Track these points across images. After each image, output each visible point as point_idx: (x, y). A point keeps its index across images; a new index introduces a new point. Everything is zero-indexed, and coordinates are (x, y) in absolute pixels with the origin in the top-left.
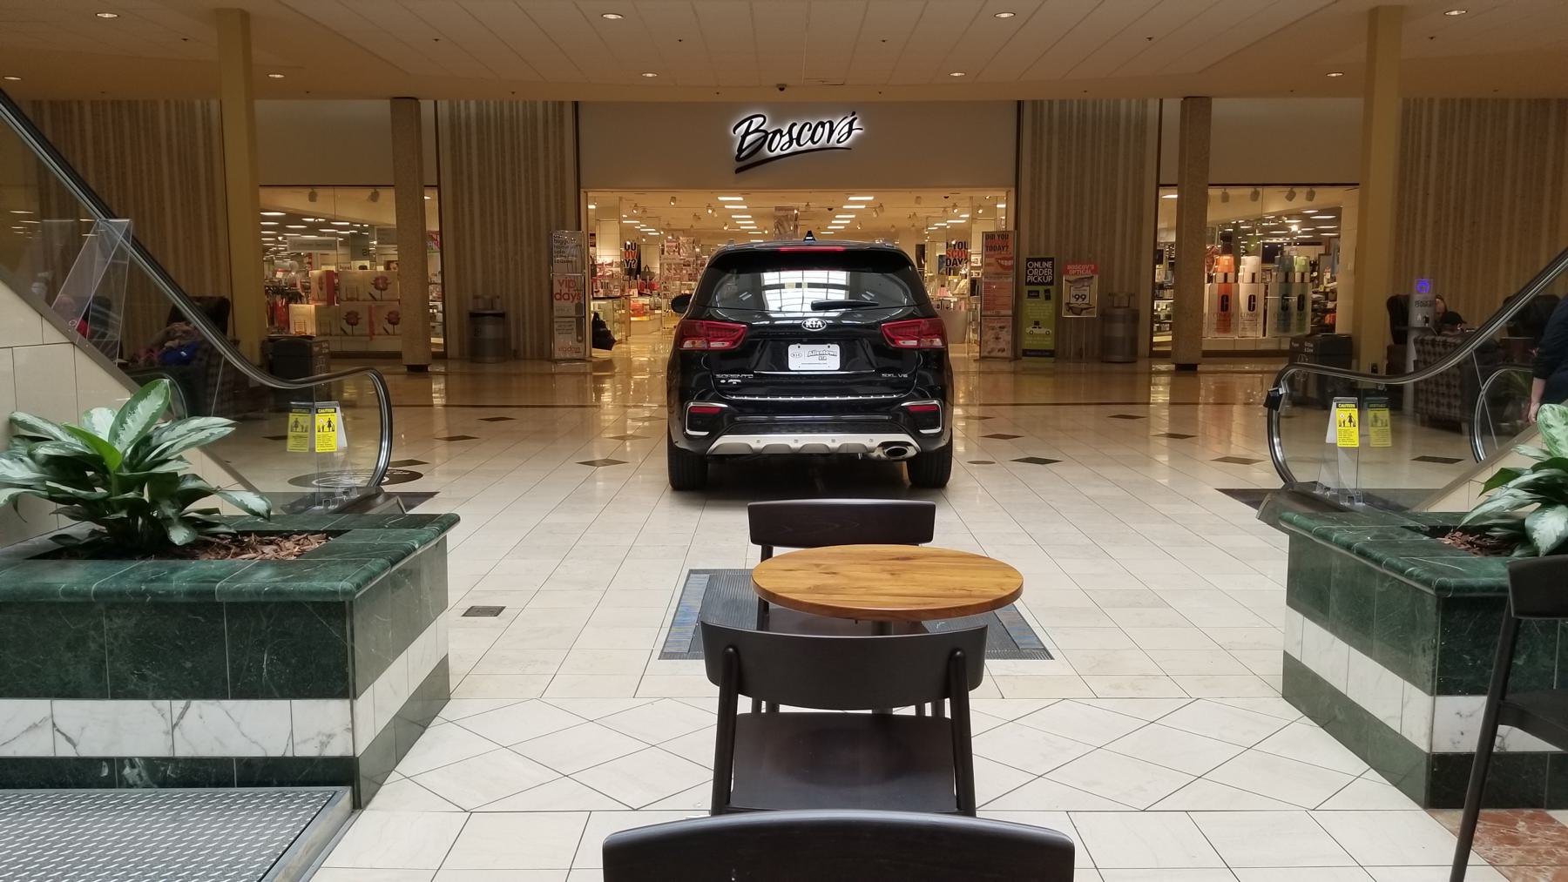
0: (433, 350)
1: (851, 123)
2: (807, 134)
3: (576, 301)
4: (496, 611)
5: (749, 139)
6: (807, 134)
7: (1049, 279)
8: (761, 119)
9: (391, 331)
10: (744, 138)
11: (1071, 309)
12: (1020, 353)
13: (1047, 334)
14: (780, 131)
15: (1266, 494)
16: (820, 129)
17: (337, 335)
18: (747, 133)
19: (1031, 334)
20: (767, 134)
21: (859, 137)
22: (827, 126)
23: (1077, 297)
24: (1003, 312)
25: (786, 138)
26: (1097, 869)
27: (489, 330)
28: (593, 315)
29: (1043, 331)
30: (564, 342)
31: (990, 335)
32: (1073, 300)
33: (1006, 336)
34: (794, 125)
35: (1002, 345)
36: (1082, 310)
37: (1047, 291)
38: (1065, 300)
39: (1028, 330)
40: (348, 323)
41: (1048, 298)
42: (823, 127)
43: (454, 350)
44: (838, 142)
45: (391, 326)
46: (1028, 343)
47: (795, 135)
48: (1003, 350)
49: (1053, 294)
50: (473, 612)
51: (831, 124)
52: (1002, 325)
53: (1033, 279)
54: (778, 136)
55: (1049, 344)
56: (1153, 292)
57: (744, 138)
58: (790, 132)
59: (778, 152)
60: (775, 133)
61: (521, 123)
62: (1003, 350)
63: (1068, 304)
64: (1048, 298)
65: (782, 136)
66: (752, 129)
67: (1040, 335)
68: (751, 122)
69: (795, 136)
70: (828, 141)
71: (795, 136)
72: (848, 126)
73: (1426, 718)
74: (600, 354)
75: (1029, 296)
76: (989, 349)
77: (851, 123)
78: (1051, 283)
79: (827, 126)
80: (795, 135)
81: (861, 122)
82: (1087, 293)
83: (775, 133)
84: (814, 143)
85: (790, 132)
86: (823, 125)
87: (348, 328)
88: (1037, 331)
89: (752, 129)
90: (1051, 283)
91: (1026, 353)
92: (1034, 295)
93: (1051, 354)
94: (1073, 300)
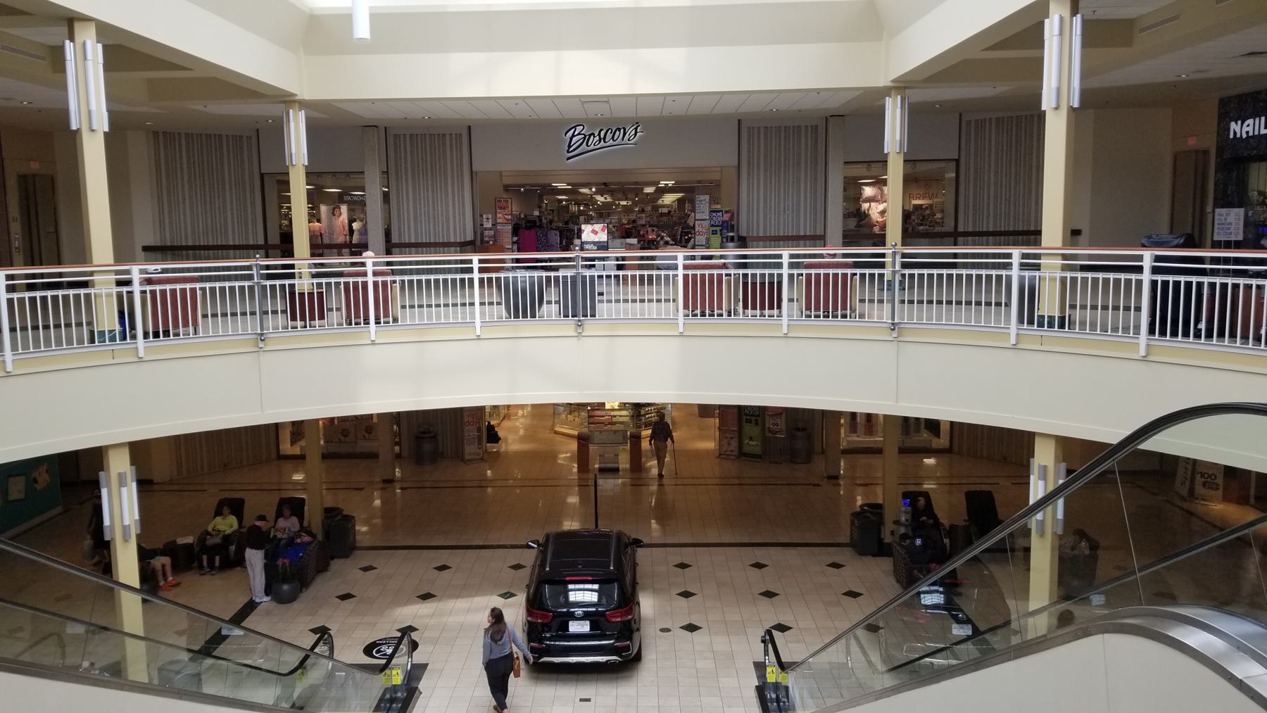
1: (636, 129)
2: (609, 135)
3: (477, 425)
5: (575, 139)
6: (609, 135)
7: (757, 413)
8: (582, 127)
9: (367, 437)
10: (571, 139)
11: (770, 431)
12: (742, 454)
13: (757, 445)
16: (618, 132)
17: (336, 442)
18: (573, 136)
19: (748, 444)
20: (585, 136)
21: (640, 136)
22: (622, 130)
23: (773, 424)
24: (733, 429)
26: (836, 628)
27: (427, 447)
28: (487, 423)
29: (754, 443)
30: (470, 450)
31: (725, 442)
32: (771, 426)
33: (734, 444)
34: (602, 130)
35: (732, 448)
36: (777, 432)
37: (757, 420)
38: (767, 426)
39: (746, 442)
40: (343, 435)
41: (757, 424)
42: (620, 131)
43: (405, 453)
44: (629, 140)
45: (367, 434)
46: (746, 449)
47: (602, 136)
48: (733, 451)
49: (760, 423)
52: (732, 436)
53: (748, 412)
54: (592, 137)
55: (758, 451)
57: (571, 139)
58: (599, 135)
59: (592, 147)
60: (590, 136)
62: (733, 451)
63: (769, 428)
64: (757, 424)
65: (594, 137)
66: (576, 133)
67: (753, 445)
68: (576, 129)
69: (602, 136)
71: (602, 136)
72: (634, 131)
74: (493, 447)
75: (746, 422)
76: (724, 450)
77: (636, 129)
78: (758, 416)
79: (622, 130)
80: (602, 136)
82: (779, 422)
83: (590, 136)
84: (614, 141)
85: (599, 135)
86: (619, 130)
87: (343, 438)
88: (750, 442)
89: (576, 133)
90: (758, 416)
91: (746, 455)
92: (749, 421)
93: (760, 457)
94: (771, 426)
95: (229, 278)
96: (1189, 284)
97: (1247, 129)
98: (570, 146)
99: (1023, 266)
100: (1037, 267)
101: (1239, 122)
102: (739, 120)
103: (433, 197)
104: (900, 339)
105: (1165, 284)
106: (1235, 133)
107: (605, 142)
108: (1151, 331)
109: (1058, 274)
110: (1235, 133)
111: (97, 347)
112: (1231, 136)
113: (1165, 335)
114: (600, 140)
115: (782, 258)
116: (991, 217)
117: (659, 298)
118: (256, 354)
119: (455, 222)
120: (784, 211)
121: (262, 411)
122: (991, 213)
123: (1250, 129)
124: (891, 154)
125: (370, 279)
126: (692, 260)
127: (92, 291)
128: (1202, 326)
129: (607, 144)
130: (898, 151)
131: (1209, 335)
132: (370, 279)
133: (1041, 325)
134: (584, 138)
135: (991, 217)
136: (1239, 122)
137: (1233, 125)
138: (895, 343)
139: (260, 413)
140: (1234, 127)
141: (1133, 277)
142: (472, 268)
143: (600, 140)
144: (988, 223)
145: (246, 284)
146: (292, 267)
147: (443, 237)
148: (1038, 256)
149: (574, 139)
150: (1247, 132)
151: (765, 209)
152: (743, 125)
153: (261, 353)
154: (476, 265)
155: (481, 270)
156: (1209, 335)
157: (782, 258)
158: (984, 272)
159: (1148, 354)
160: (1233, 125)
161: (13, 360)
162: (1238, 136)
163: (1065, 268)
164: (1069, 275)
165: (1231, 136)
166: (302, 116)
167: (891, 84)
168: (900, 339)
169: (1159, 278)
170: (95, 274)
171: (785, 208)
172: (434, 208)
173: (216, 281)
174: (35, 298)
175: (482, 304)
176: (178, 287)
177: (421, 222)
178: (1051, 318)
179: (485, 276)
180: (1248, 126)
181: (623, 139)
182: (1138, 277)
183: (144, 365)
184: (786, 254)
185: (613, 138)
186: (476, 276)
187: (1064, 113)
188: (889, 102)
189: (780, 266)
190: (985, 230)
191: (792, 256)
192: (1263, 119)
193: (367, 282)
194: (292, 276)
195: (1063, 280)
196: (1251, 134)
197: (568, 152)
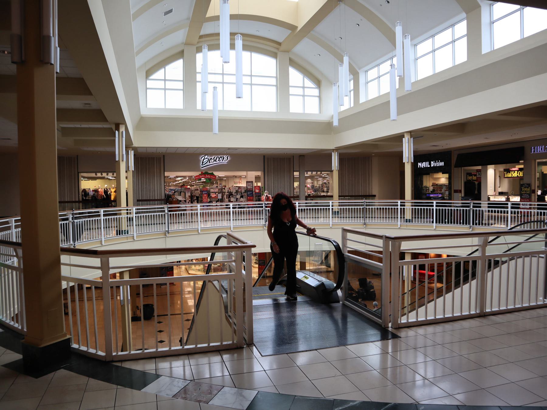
0: (279, 111)
1: (227, 157)
2: (218, 159)
4: (171, 11)
6: (218, 159)
8: (207, 156)
10: (203, 160)
14: (212, 159)
15: (403, 136)
16: (221, 158)
18: (204, 159)
20: (209, 159)
21: (229, 160)
22: (222, 158)
25: (213, 160)
44: (225, 161)
50: (223, 65)
51: (223, 157)
56: (165, 187)
57: (203, 160)
58: (214, 159)
59: (211, 163)
60: (210, 159)
61: (156, 174)
65: (212, 160)
69: (215, 160)
70: (223, 161)
71: (215, 160)
73: (220, 372)
77: (227, 157)
79: (222, 158)
81: (230, 157)
84: (219, 161)
85: (214, 159)
86: (221, 157)
95: (150, 212)
96: (442, 209)
97: (424, 165)
98: (203, 163)
99: (401, 205)
100: (404, 206)
101: (421, 163)
102: (264, 156)
103: (149, 182)
104: (366, 227)
105: (415, 209)
106: (420, 166)
107: (216, 161)
108: (436, 222)
109: (411, 208)
110: (420, 166)
111: (121, 236)
112: (419, 167)
113: (455, 223)
114: (214, 161)
115: (433, 204)
116: (347, 191)
117: (255, 218)
118: (263, 231)
119: (157, 191)
120: (280, 188)
121: (166, 258)
122: (347, 189)
123: (424, 165)
124: (335, 170)
125: (435, 208)
126: (531, 204)
127: (121, 216)
128: (447, 220)
129: (210, 164)
130: (337, 169)
131: (448, 223)
132: (435, 208)
133: (407, 222)
134: (208, 160)
135: (347, 191)
136: (421, 163)
137: (419, 163)
138: (365, 229)
139: (166, 259)
140: (419, 164)
141: (431, 208)
142: (433, 205)
143: (214, 161)
144: (346, 192)
145: (361, 207)
146: (480, 204)
147: (153, 197)
148: (404, 203)
149: (204, 160)
150: (424, 166)
151: (273, 187)
152: (266, 157)
153: (167, 238)
154: (435, 204)
155: (437, 206)
156: (448, 223)
157: (433, 204)
158: (345, 207)
159: (436, 228)
160: (419, 163)
161: (104, 240)
162: (421, 167)
163: (412, 206)
164: (414, 207)
165: (419, 167)
166: (133, 152)
167: (335, 148)
168: (366, 227)
169: (438, 208)
170: (122, 210)
171: (280, 187)
172: (149, 185)
173: (144, 213)
174: (528, 212)
175: (233, 220)
176: (441, 208)
177: (144, 191)
178: (409, 220)
179: (513, 210)
180: (424, 164)
181: (223, 161)
182: (433, 208)
183: (200, 235)
184: (435, 202)
185: (219, 160)
186: (509, 210)
187: (410, 164)
188: (333, 154)
189: (433, 206)
190: (345, 195)
191: (437, 203)
192: (428, 162)
193: (398, 208)
194: (480, 207)
195: (412, 209)
196: (425, 167)
197: (202, 165)
